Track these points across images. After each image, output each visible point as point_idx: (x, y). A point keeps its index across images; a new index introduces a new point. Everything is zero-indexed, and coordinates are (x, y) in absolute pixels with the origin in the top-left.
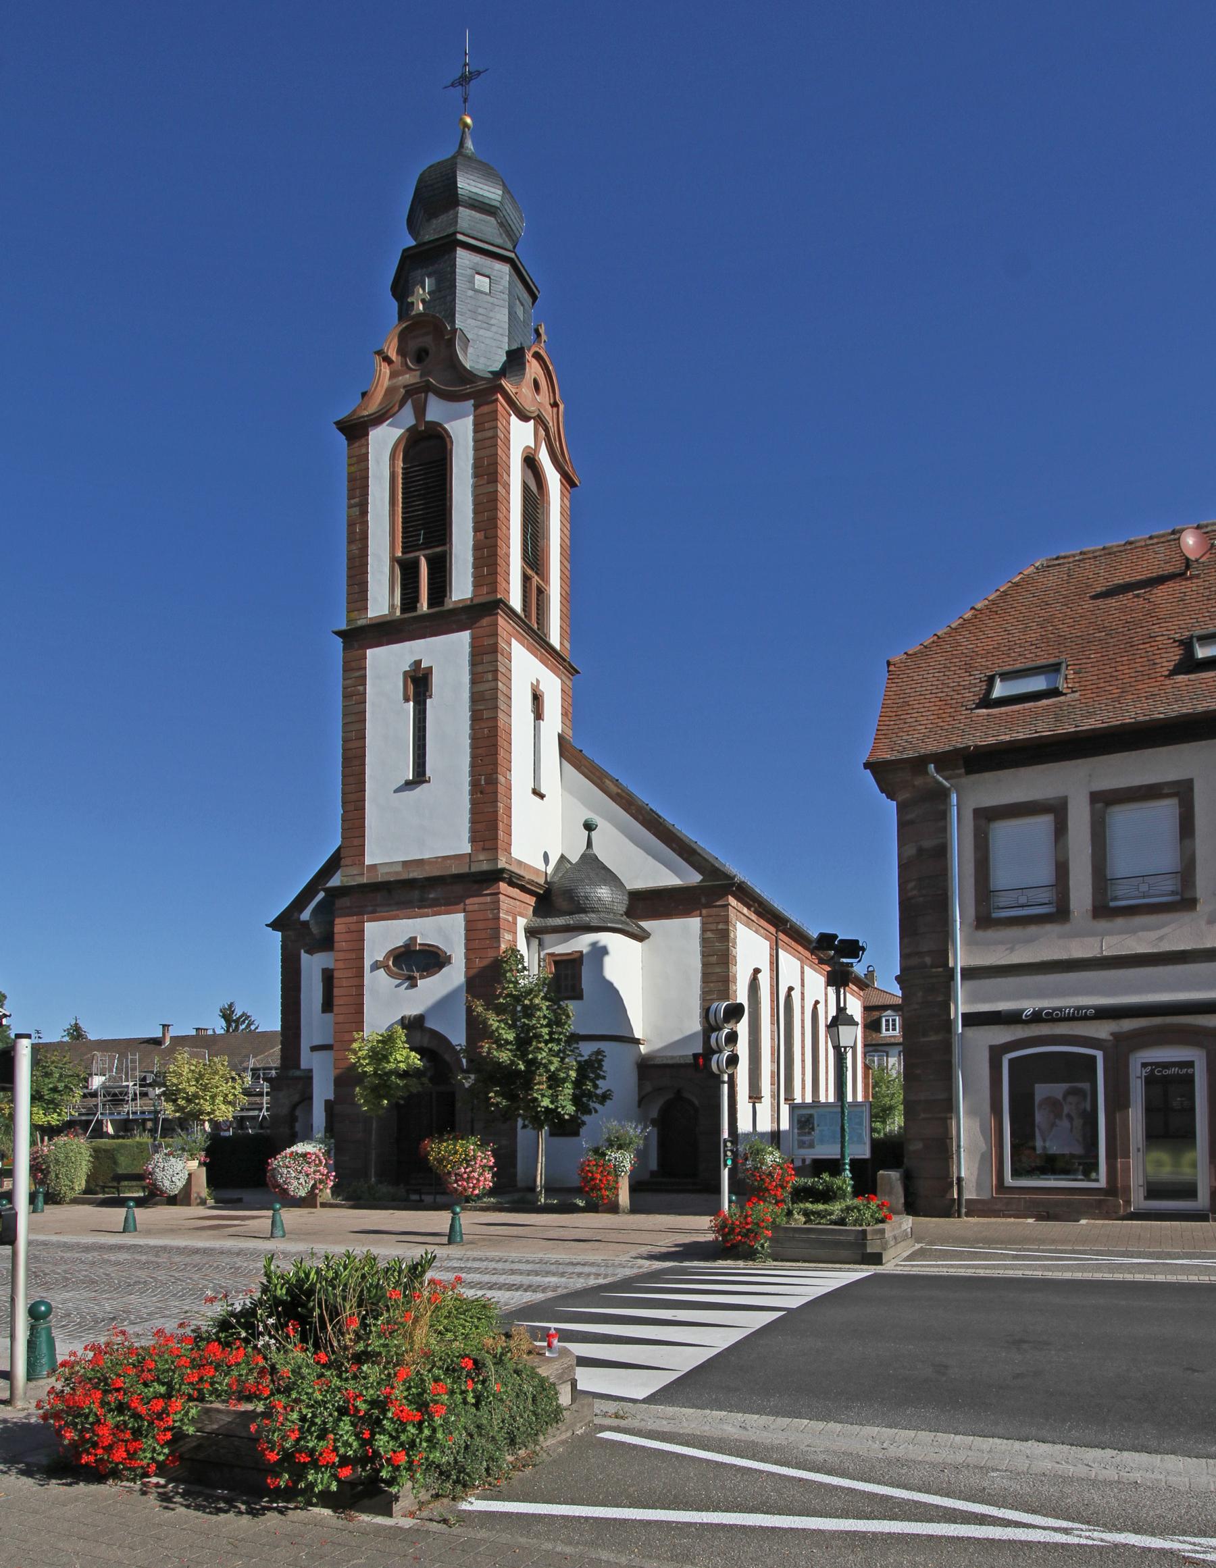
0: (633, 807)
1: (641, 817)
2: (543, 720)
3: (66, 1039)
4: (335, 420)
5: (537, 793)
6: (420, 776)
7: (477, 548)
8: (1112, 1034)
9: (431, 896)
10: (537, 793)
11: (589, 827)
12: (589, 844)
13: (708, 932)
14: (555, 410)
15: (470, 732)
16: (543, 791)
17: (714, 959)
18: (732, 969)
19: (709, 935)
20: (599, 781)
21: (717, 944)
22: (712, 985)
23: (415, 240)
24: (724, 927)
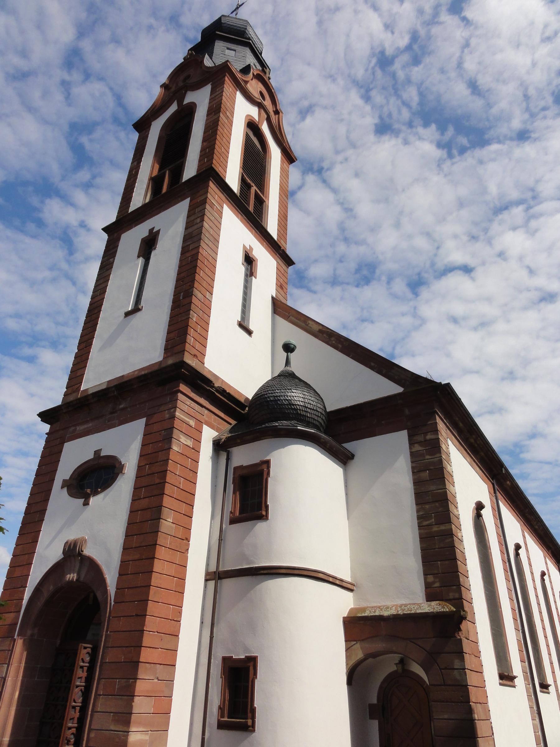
0: (333, 339)
1: (340, 346)
2: (256, 278)
3: (18, 535)
4: (515, 688)
5: (244, 326)
6: (137, 309)
7: (203, 150)
8: (232, 484)
9: (122, 406)
10: (244, 326)
11: (288, 348)
12: (288, 363)
13: (416, 445)
14: (277, 116)
15: (178, 269)
16: (251, 327)
17: (425, 475)
18: (449, 486)
19: (417, 448)
20: (303, 324)
21: (428, 457)
22: (427, 506)
23: (282, 249)
24: (433, 437)
